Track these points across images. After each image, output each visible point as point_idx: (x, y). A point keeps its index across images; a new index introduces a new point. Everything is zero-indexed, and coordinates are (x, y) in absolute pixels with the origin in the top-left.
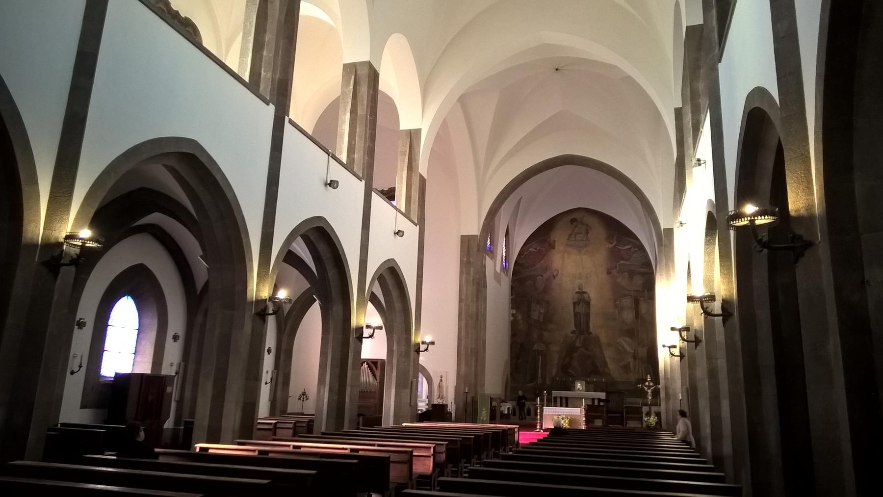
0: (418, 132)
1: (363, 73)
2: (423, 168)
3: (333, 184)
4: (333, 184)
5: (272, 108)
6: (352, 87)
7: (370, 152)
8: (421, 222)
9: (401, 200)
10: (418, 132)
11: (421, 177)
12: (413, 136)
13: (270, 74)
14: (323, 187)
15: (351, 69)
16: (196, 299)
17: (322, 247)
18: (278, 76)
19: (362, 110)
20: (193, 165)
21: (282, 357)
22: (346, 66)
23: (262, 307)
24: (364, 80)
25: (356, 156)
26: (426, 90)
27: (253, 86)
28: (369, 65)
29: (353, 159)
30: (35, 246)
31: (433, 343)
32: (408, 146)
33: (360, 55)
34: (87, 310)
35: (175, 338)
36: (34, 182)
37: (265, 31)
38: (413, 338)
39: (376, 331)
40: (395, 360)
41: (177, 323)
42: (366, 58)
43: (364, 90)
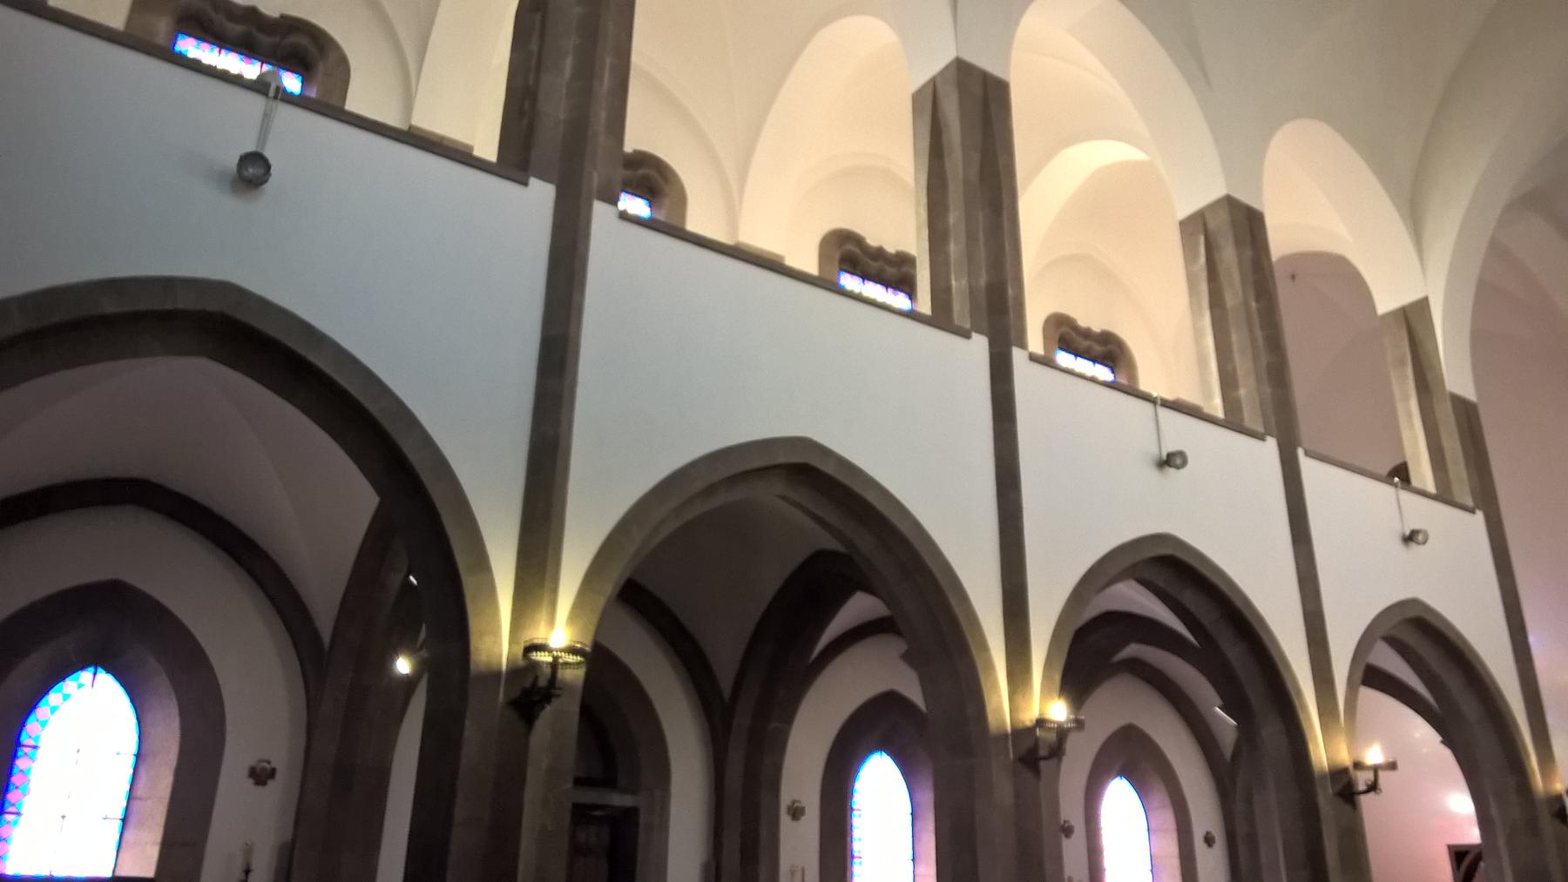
0: (1422, 305)
1: (1220, 222)
2: (1458, 378)
3: (1171, 461)
4: (1171, 461)
5: (1479, 516)
6: (1202, 259)
7: (1277, 373)
8: (1486, 500)
9: (1423, 474)
10: (1422, 305)
11: (1460, 404)
12: (1413, 319)
13: (964, 282)
14: (1154, 473)
15: (1196, 227)
16: (1227, 776)
17: (1189, 598)
18: (983, 281)
19: (1233, 295)
20: (1171, 567)
21: (1242, 850)
22: (1183, 224)
23: (1027, 744)
24: (1231, 242)
25: (1242, 392)
26: (1415, 217)
27: (1233, 422)
28: (1229, 202)
29: (1238, 401)
30: (1006, 735)
31: (1392, 766)
32: (1406, 342)
33: (1200, 188)
34: (1071, 811)
35: (1209, 840)
36: (984, 647)
37: (945, 208)
38: (1538, 782)
39: (1381, 774)
40: (1501, 842)
41: (1205, 814)
42: (1217, 191)
43: (1229, 255)
